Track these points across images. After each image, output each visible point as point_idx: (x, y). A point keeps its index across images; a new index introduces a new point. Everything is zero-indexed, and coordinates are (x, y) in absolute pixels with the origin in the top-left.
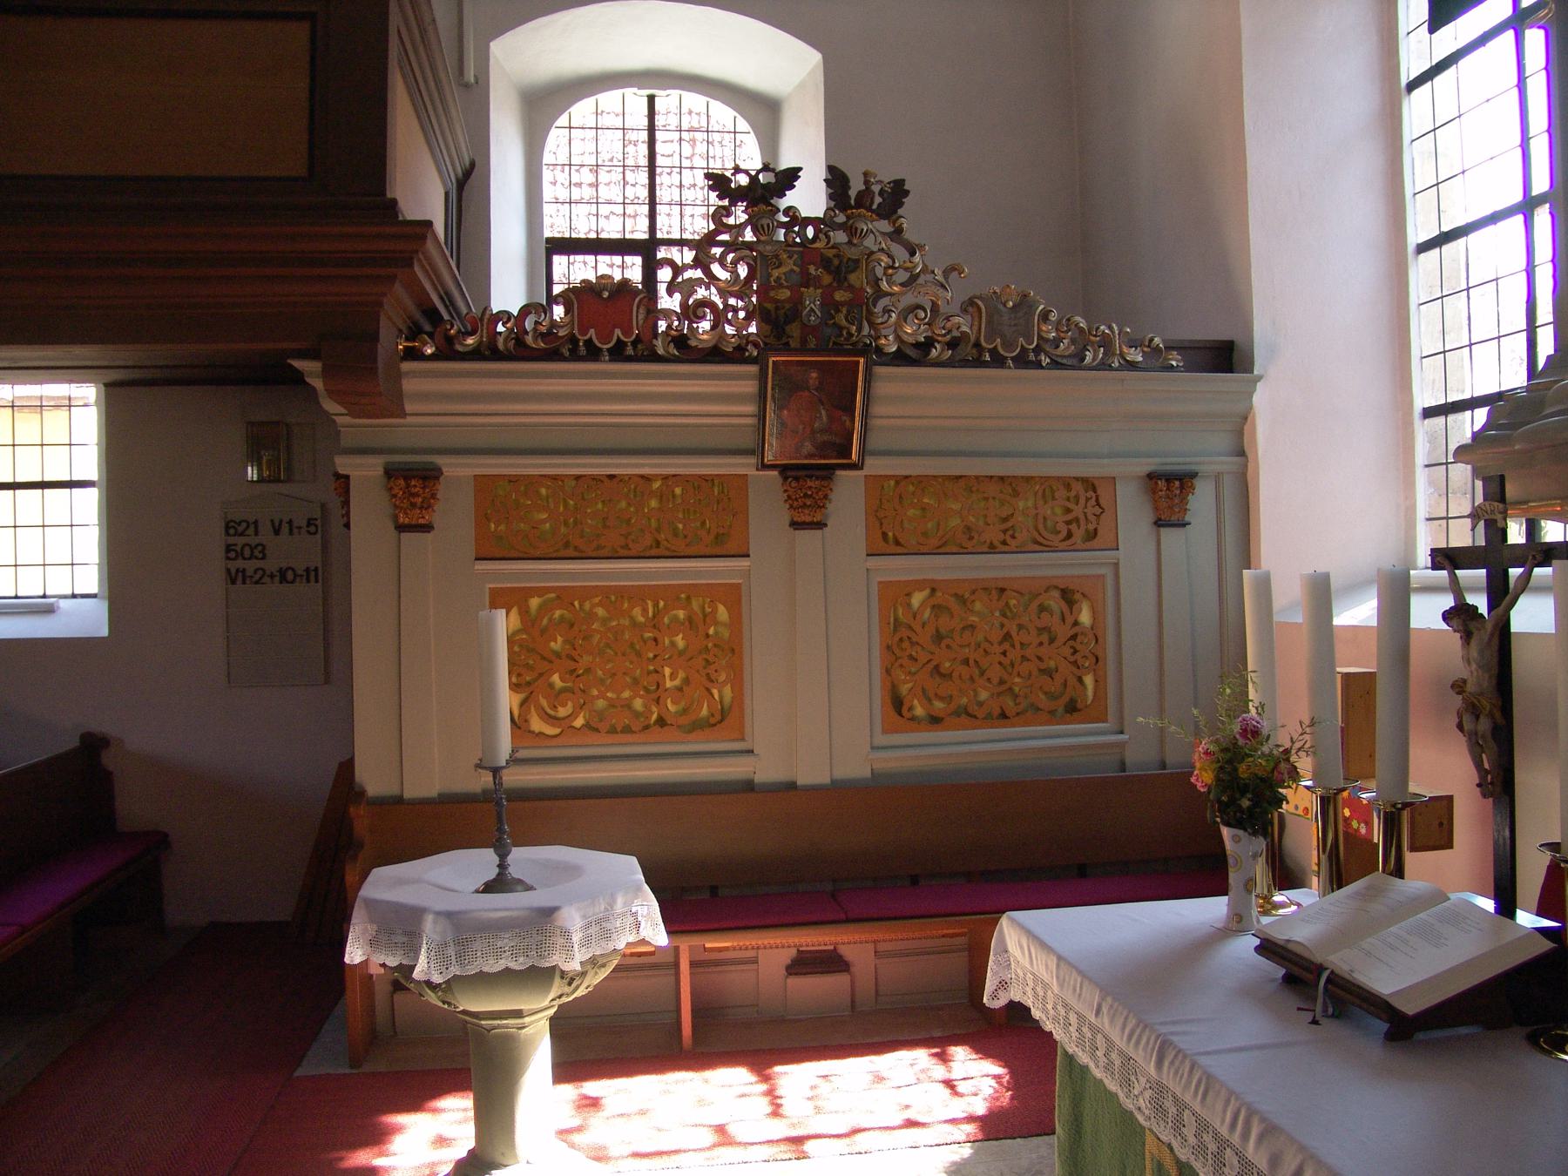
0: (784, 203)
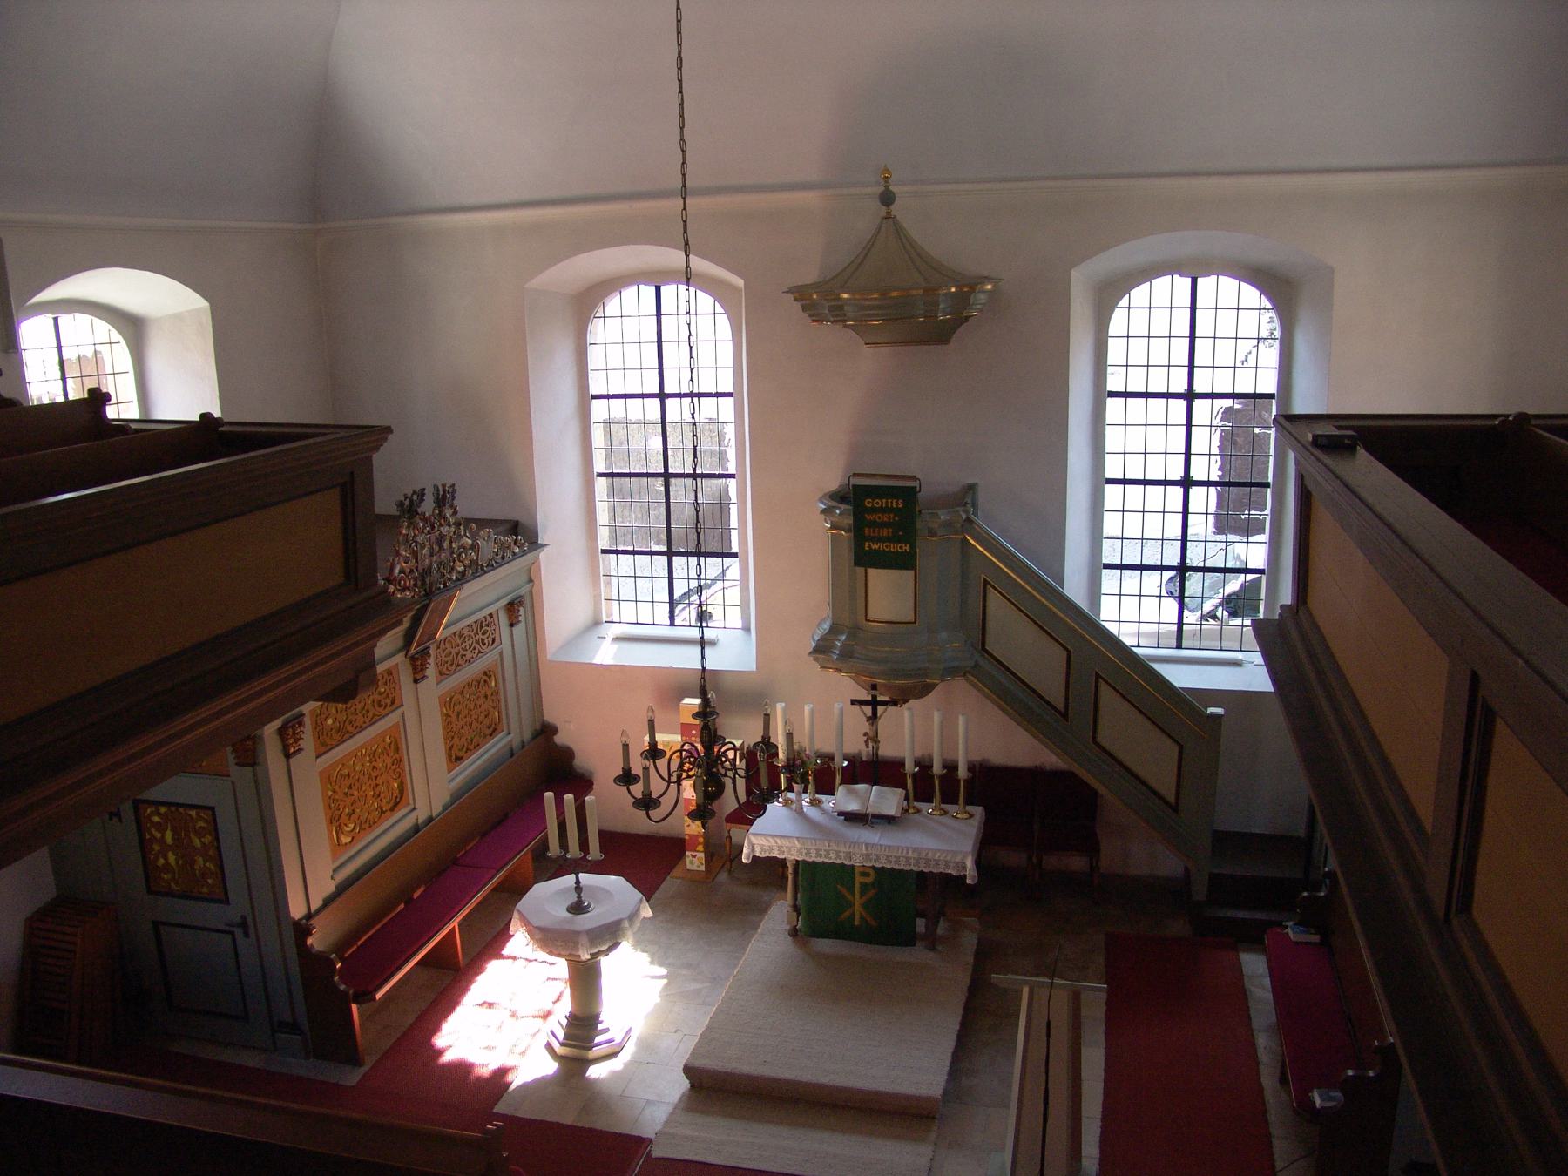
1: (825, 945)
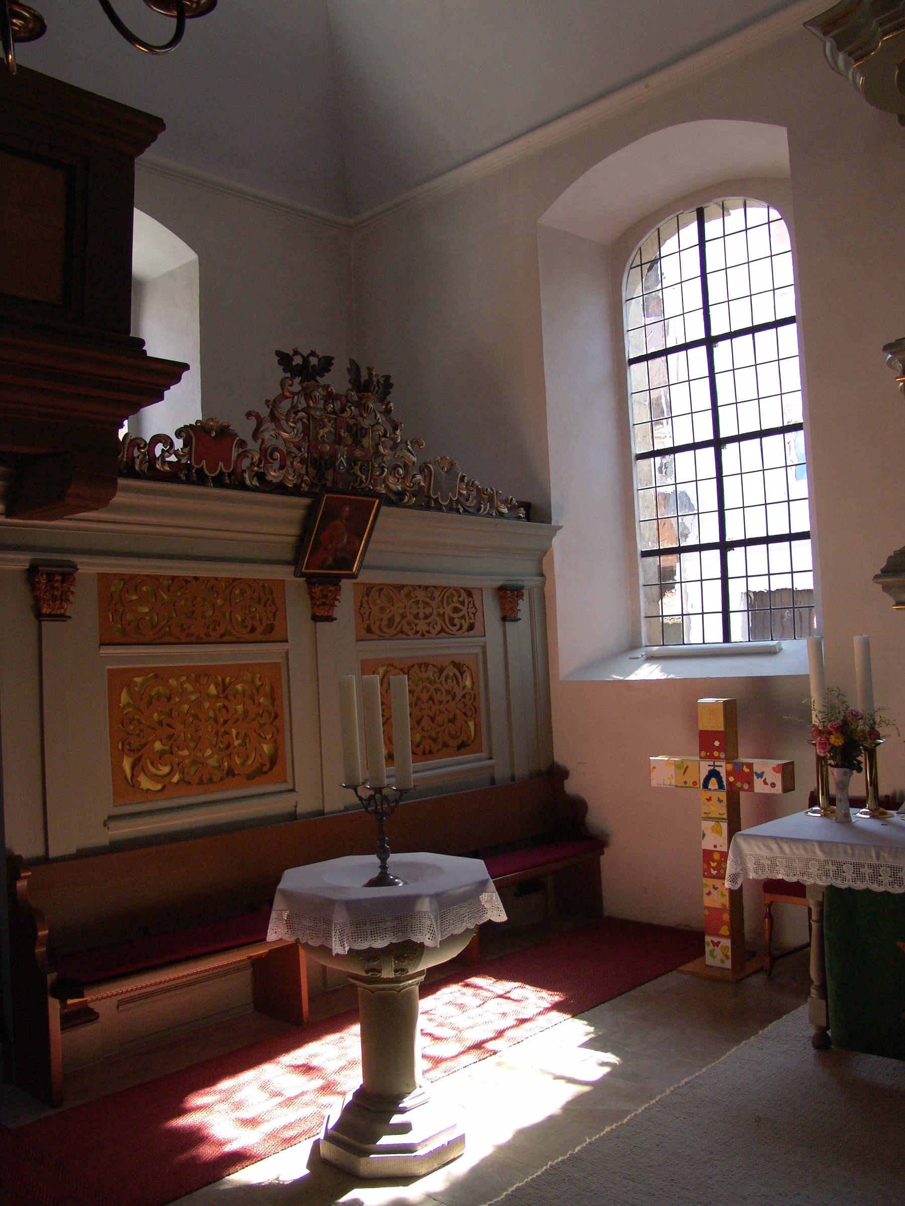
0: (322, 381)
1: (874, 1068)
